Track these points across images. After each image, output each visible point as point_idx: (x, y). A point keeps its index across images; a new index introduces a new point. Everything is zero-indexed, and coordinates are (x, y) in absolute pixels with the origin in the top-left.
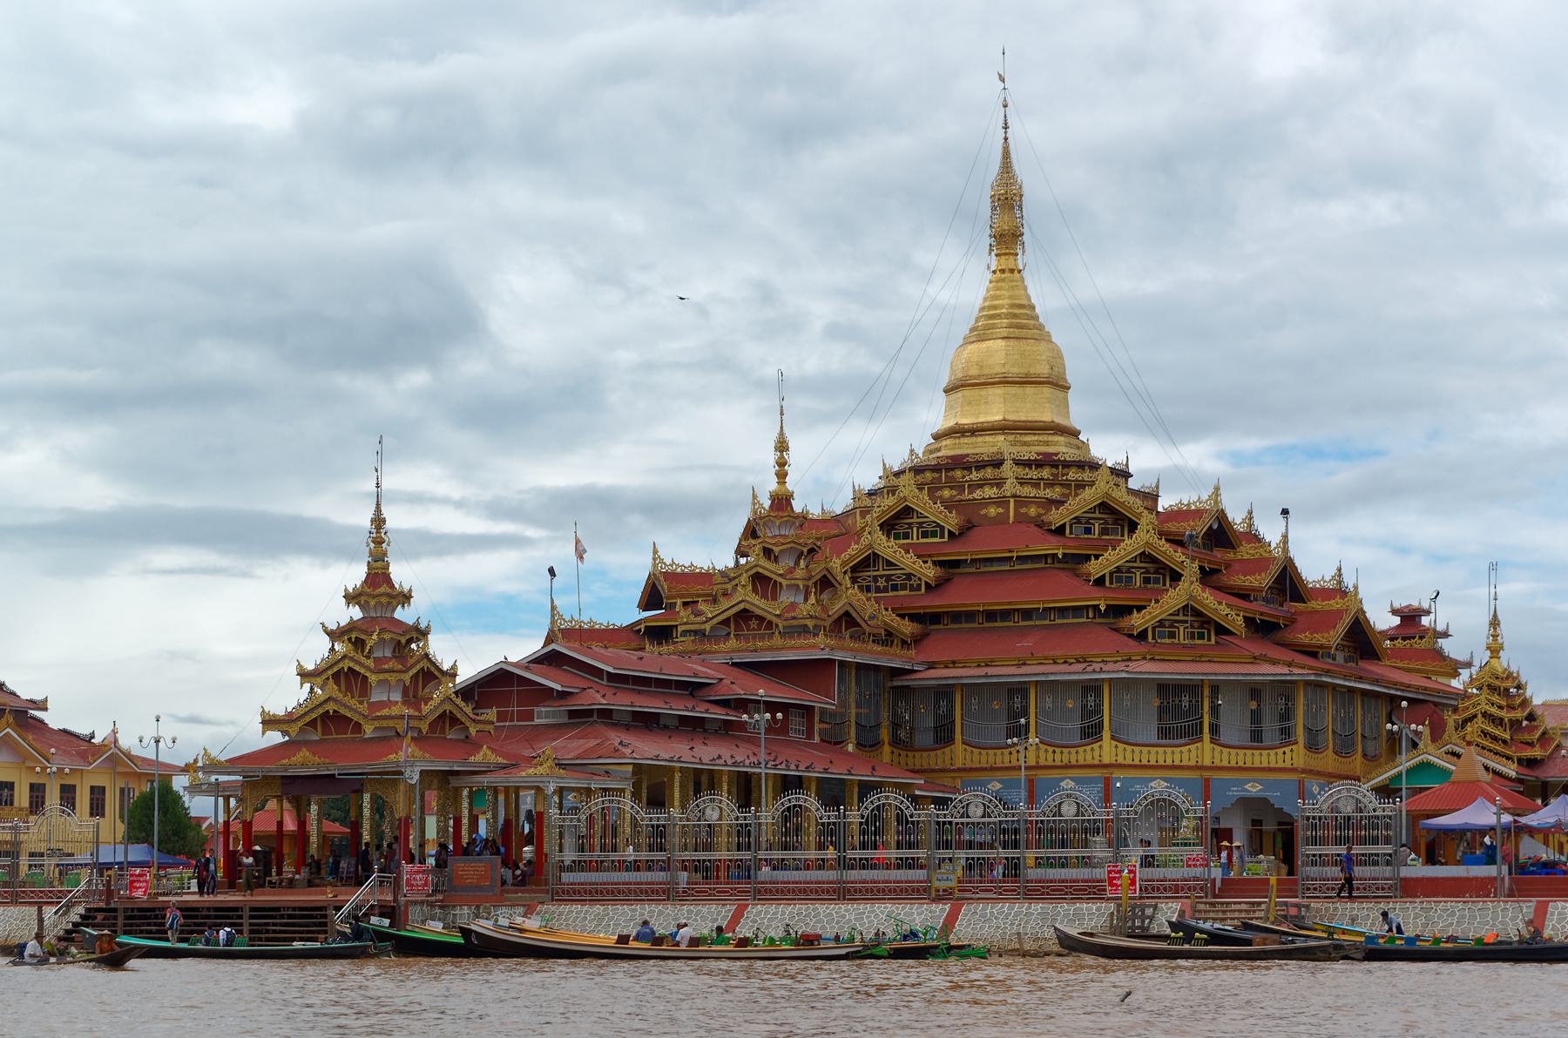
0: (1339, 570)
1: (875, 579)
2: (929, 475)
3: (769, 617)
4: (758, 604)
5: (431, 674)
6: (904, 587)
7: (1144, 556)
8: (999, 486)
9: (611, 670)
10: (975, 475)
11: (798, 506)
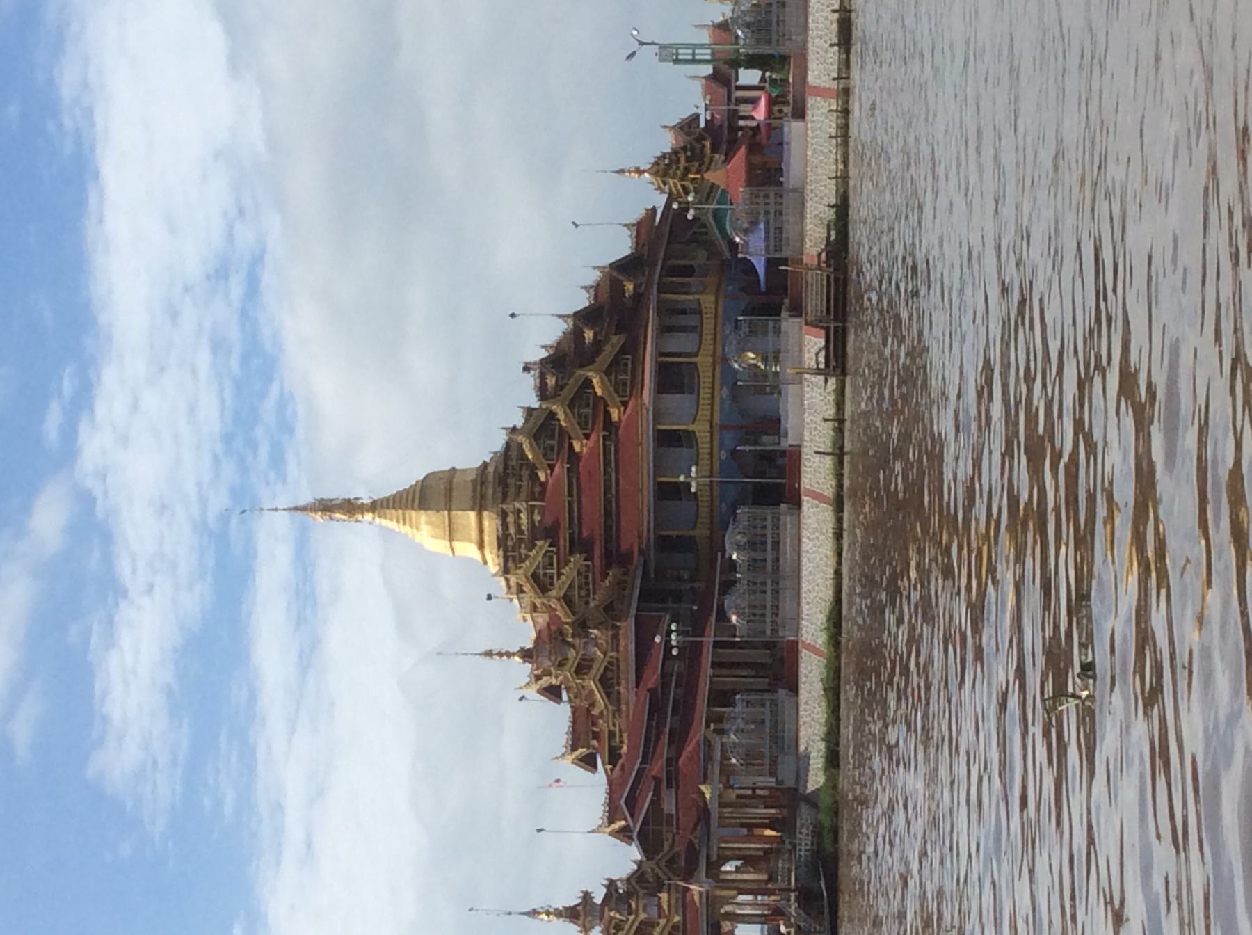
0: (560, 316)
1: (580, 596)
2: (510, 564)
3: (605, 664)
4: (597, 669)
5: (638, 877)
6: (587, 577)
7: (571, 405)
8: (519, 511)
9: (639, 761)
10: (512, 530)
11: (529, 645)
